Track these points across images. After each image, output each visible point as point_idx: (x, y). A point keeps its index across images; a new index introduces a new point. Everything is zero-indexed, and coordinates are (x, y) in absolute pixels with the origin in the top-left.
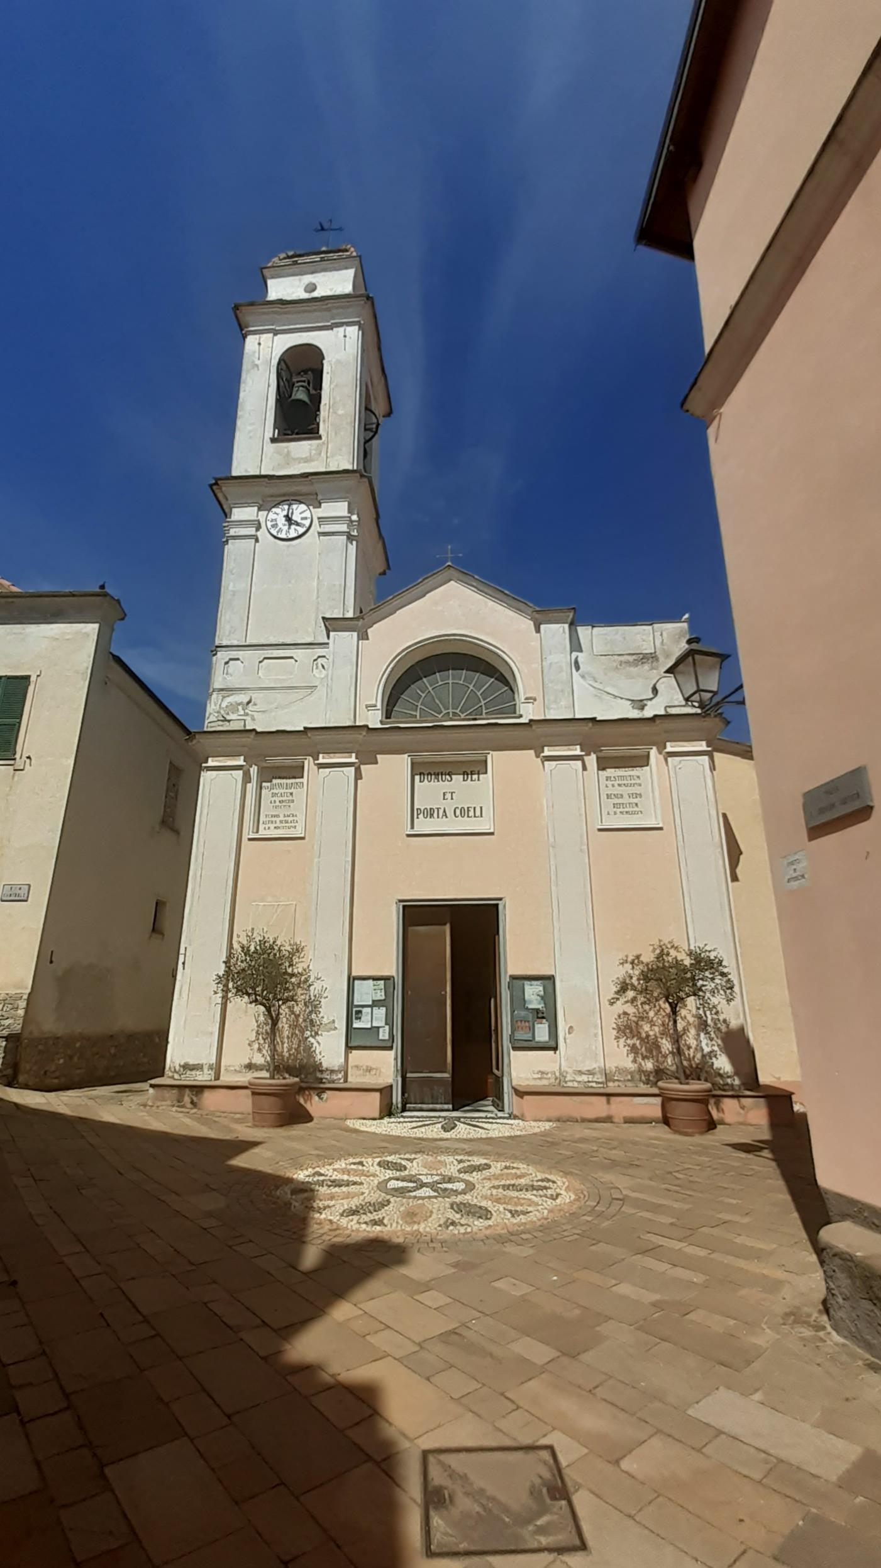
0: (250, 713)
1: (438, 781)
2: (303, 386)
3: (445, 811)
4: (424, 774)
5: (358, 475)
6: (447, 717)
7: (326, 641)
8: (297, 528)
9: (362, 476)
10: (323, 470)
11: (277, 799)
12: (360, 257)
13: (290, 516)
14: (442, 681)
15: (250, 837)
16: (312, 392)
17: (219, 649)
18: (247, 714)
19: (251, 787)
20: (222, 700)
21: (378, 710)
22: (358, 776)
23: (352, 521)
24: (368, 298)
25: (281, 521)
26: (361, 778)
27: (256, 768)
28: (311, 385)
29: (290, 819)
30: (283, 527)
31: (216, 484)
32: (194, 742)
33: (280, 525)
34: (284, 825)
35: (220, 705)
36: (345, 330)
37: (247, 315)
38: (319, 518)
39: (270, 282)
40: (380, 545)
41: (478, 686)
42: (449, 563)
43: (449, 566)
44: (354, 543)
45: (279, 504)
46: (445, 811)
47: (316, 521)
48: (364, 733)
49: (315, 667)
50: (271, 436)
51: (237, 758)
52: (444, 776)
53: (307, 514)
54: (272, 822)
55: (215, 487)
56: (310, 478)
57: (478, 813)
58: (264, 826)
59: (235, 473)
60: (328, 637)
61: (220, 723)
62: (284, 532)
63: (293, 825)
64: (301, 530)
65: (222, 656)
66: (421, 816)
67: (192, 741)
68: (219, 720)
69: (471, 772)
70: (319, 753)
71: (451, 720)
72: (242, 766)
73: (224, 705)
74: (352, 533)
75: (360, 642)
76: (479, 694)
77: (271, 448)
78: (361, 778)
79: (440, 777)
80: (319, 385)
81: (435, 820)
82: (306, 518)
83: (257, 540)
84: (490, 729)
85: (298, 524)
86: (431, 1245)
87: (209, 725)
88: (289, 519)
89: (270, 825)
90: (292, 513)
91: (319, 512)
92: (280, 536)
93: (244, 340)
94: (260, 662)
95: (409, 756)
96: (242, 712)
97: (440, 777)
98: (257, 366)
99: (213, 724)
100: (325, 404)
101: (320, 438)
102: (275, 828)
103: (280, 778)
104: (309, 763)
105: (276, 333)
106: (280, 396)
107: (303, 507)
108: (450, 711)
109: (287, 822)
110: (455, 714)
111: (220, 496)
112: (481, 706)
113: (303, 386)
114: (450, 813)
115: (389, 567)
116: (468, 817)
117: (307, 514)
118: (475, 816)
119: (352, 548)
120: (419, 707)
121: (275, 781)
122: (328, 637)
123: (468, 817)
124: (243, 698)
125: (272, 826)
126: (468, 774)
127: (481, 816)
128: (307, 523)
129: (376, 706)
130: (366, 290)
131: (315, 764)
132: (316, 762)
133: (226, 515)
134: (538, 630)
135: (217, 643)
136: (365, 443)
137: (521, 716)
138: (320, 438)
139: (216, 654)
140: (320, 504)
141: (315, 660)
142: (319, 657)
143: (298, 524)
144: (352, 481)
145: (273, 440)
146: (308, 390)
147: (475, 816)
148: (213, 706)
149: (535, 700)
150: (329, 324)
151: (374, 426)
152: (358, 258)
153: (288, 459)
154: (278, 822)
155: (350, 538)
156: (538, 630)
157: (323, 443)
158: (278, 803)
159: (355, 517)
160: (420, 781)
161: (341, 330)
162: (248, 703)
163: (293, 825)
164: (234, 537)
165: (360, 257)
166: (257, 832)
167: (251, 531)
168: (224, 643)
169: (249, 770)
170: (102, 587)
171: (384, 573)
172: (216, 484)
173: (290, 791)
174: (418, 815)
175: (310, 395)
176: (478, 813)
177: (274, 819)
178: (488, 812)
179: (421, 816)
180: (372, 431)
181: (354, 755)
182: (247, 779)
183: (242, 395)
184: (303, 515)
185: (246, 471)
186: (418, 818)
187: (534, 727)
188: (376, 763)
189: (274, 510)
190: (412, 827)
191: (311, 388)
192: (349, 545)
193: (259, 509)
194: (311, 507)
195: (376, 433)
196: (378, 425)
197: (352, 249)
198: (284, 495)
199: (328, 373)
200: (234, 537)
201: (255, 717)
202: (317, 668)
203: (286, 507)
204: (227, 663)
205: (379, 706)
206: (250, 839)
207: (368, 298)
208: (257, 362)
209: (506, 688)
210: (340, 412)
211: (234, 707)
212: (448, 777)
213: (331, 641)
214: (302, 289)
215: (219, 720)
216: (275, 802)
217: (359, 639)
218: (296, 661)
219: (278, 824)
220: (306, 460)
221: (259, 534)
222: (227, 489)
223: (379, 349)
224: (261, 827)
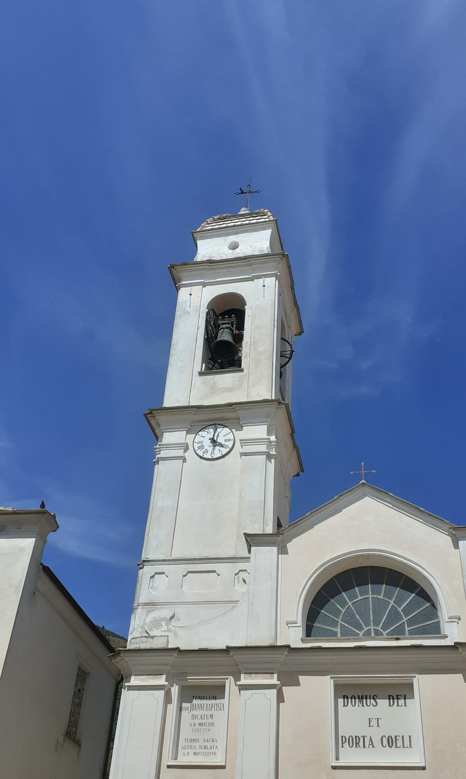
0: (173, 628)
1: (363, 706)
2: (227, 328)
3: (371, 740)
4: (347, 698)
5: (277, 403)
6: (367, 635)
7: (247, 555)
8: (221, 449)
9: (279, 403)
10: (244, 400)
11: (197, 721)
12: (276, 221)
13: (215, 439)
14: (361, 596)
15: (169, 763)
16: (236, 332)
17: (145, 563)
18: (169, 630)
19: (172, 708)
20: (146, 615)
21: (300, 627)
22: (280, 698)
23: (271, 442)
24: (283, 255)
25: (207, 444)
26: (283, 702)
27: (177, 687)
28: (234, 325)
29: (209, 744)
30: (208, 448)
31: (151, 413)
32: (118, 659)
33: (206, 447)
34: (204, 751)
35: (144, 620)
36: (264, 280)
37: (181, 272)
38: (241, 440)
39: (199, 243)
40: (295, 453)
41: (399, 602)
42: (363, 481)
43: (363, 483)
44: (273, 461)
45: (205, 428)
46: (371, 740)
47: (238, 443)
48: (286, 653)
49: (236, 581)
50: (200, 371)
51: (159, 676)
52: (368, 700)
53: (231, 436)
54: (191, 747)
55: (148, 416)
56: (234, 406)
57: (407, 743)
58: (184, 751)
59: (167, 404)
60: (249, 552)
61: (145, 639)
62: (209, 453)
63: (212, 751)
64: (225, 451)
65: (147, 570)
66: (346, 745)
67: (115, 658)
68: (142, 637)
69: (397, 696)
70: (240, 673)
71: (373, 639)
72: (164, 686)
73: (148, 621)
74: (271, 453)
75: (280, 556)
76: (400, 610)
77: (198, 380)
78: (283, 702)
79: (364, 700)
80: (240, 325)
81: (360, 750)
82: (229, 440)
83: (185, 460)
84: (415, 651)
85: (221, 445)
86: (221, 249)
87: (133, 640)
88: (214, 442)
89: (189, 750)
90: (218, 436)
91: (241, 435)
92: (205, 456)
93: (178, 291)
94: (184, 576)
95: (331, 678)
96: (165, 628)
97: (364, 700)
98: (188, 312)
99: (137, 640)
100: (247, 342)
101: (242, 370)
102: (194, 753)
103: (200, 698)
104: (230, 682)
105: (204, 285)
106: (208, 335)
107: (226, 430)
108: (372, 627)
109: (205, 747)
110: (376, 632)
111: (153, 422)
112: (404, 622)
113: (227, 328)
114: (377, 742)
115: (302, 471)
116: (396, 747)
117: (231, 436)
118: (403, 747)
119: (271, 466)
120: (340, 622)
121: (195, 702)
122: (249, 552)
123: (396, 747)
124: (166, 613)
125: (191, 751)
126: (393, 699)
127: (411, 747)
128: (230, 444)
129: (296, 623)
130: (283, 251)
131: (236, 685)
132: (238, 683)
133: (157, 438)
134: (456, 546)
135: (143, 558)
136: (281, 368)
137: (446, 637)
138: (242, 370)
139: (142, 568)
140: (242, 427)
141: (236, 574)
142: (240, 571)
143: (221, 445)
144: (272, 409)
145: (201, 374)
146: (232, 331)
147: (403, 747)
148: (137, 622)
149: (459, 619)
150: (251, 276)
151: (289, 353)
152: (275, 222)
153: (214, 390)
154: (197, 747)
155: (269, 457)
156: (456, 546)
157: (245, 375)
158: (197, 725)
159: (273, 438)
160: (344, 706)
161: (261, 281)
162: (172, 618)
163: (212, 751)
164: (164, 459)
165: (276, 221)
166: (176, 758)
167: (180, 453)
168: (151, 557)
169: (170, 689)
170: (43, 505)
171: (298, 475)
172: (151, 413)
173: (211, 713)
174: (342, 743)
175: (234, 336)
176: (407, 743)
177: (192, 744)
178: (418, 742)
179: (346, 745)
180: (287, 358)
181: (275, 676)
182: (168, 699)
183: (174, 336)
184: (227, 437)
185: (177, 401)
186: (343, 746)
187: (460, 650)
188: (298, 684)
189: (200, 433)
190: (337, 759)
191: (234, 329)
192: (268, 462)
193: (188, 433)
194: (234, 430)
195: (290, 358)
196: (292, 351)
197: (269, 214)
198: (210, 420)
199: (249, 316)
200: (164, 459)
201: (178, 633)
202: (238, 582)
203: (212, 431)
204: (152, 577)
205: (300, 623)
206: (169, 767)
207: (283, 255)
208: (188, 309)
209: (429, 604)
210: (260, 349)
211: (156, 623)
212: (372, 701)
213: (252, 555)
214: (226, 247)
215: (142, 637)
216: (195, 724)
217: (278, 554)
218: (219, 575)
219: (197, 750)
220: (230, 390)
221: (186, 454)
222: (160, 418)
223: (293, 288)
224: (180, 751)
